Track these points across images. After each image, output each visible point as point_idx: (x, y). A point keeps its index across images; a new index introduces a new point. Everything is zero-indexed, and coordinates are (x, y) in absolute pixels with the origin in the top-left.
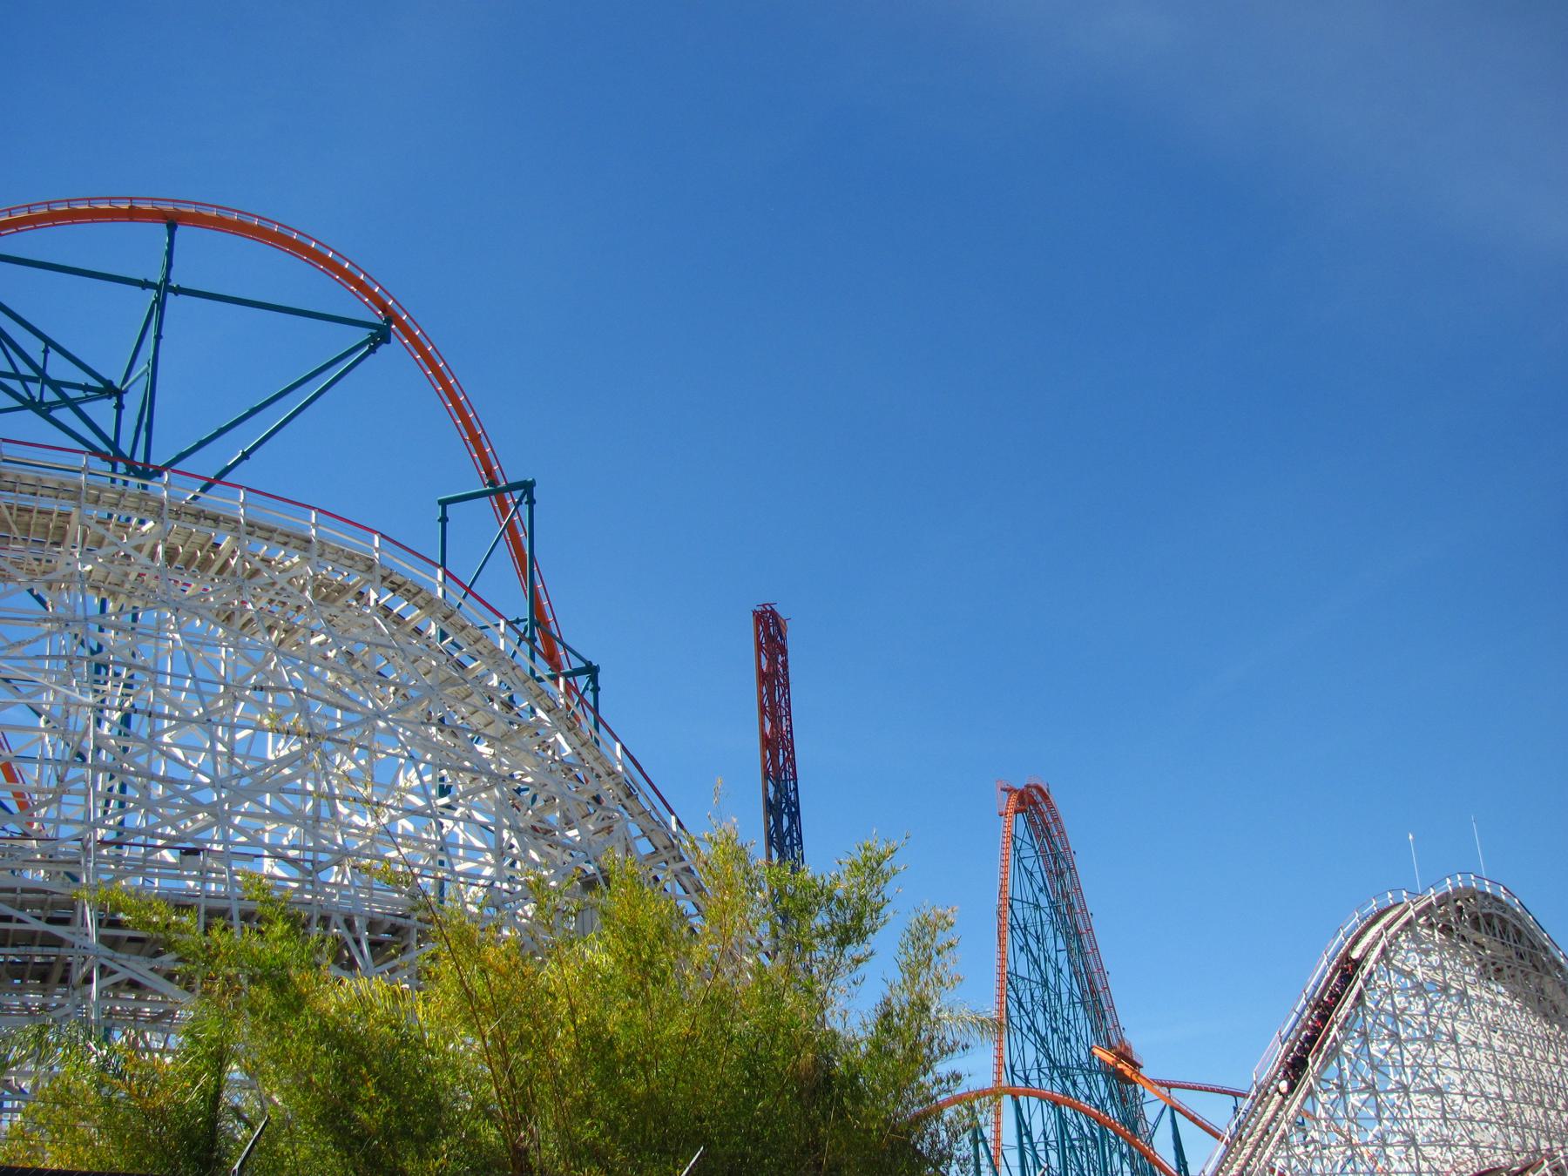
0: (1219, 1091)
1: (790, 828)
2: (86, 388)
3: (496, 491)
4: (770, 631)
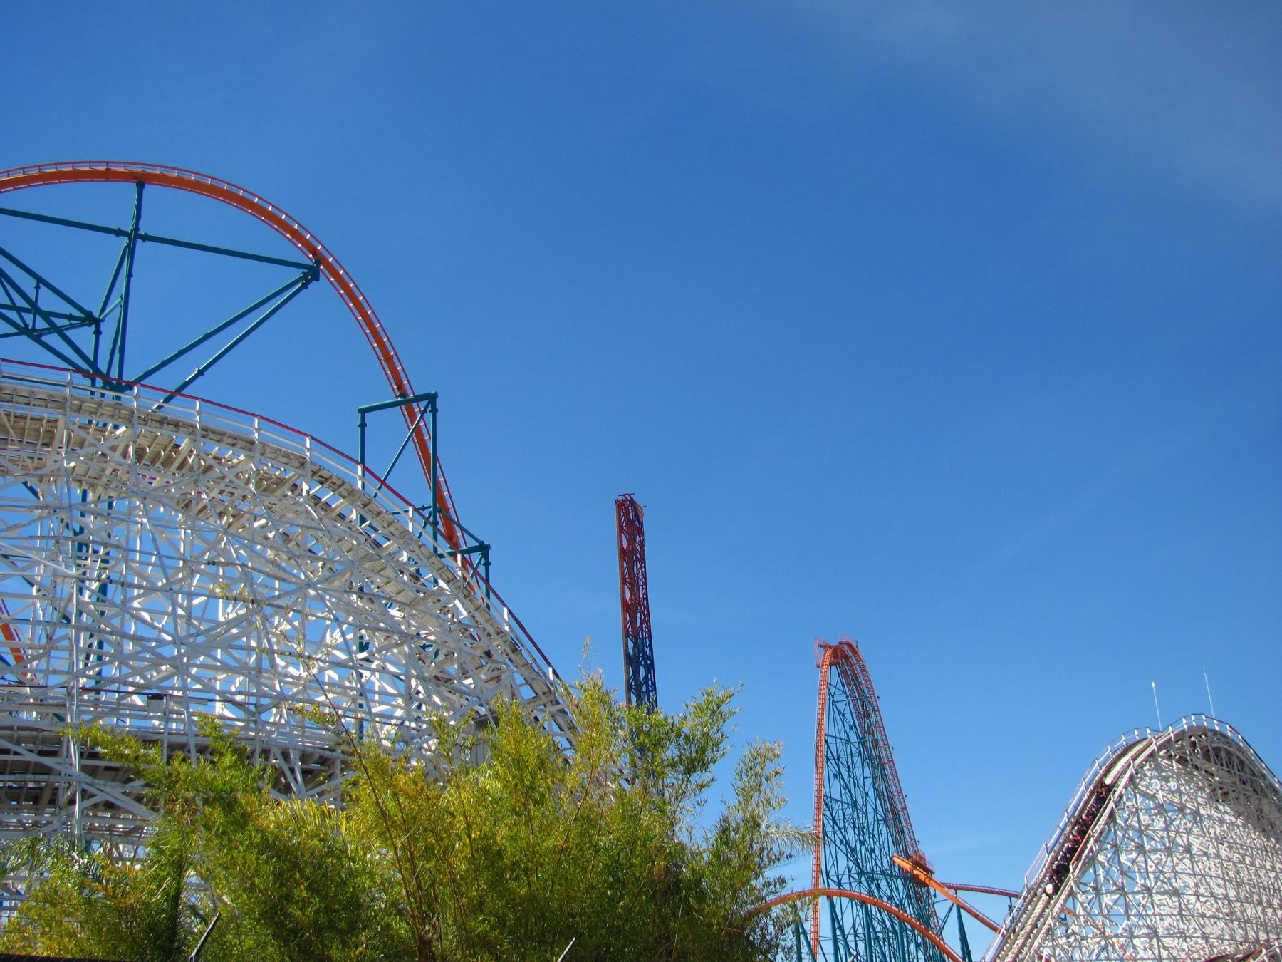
0: (997, 893)
1: (646, 677)
2: (70, 317)
3: (405, 402)
4: (630, 516)
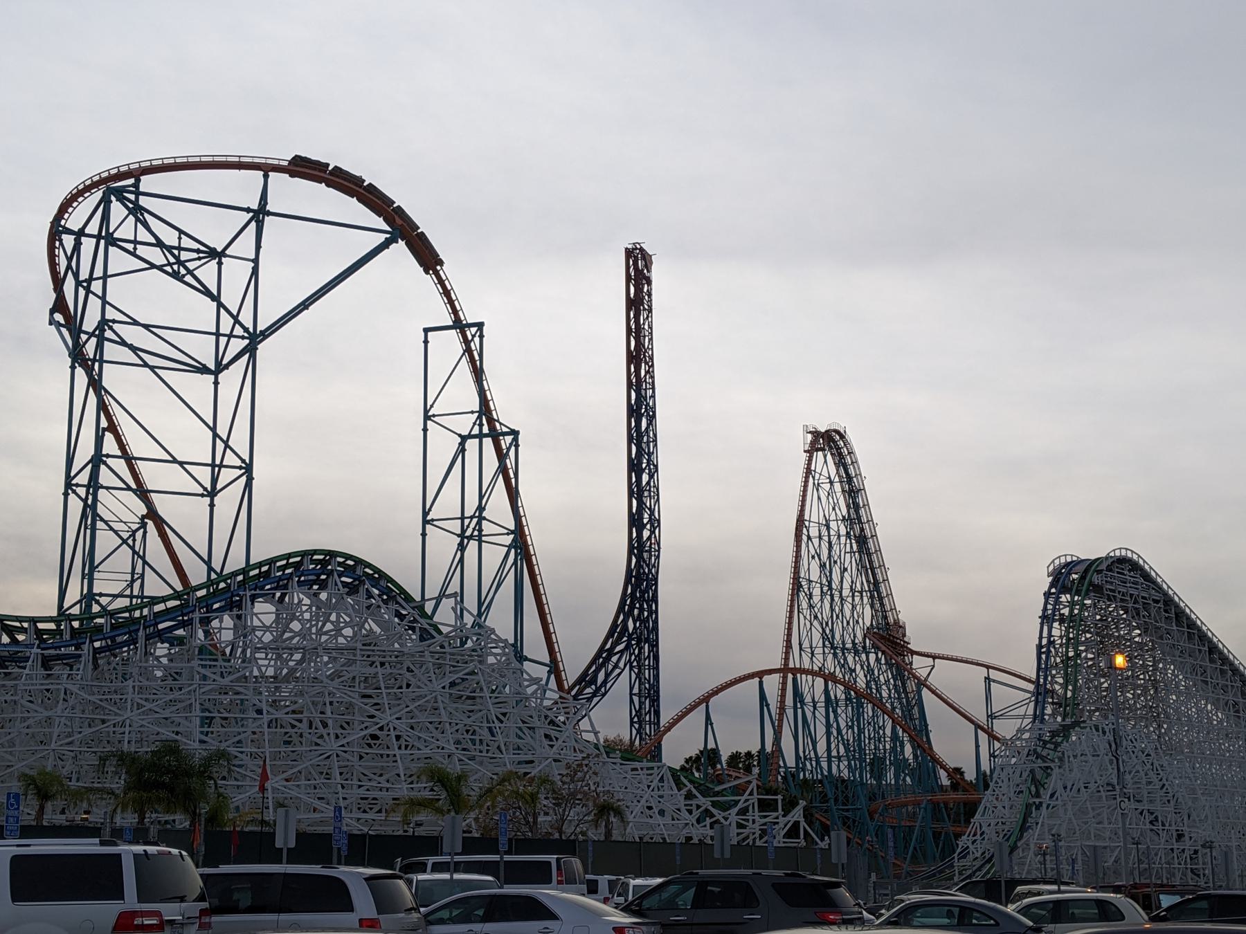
0: (966, 662)
1: (647, 429)
2: (198, 251)
3: (459, 324)
4: (638, 266)
